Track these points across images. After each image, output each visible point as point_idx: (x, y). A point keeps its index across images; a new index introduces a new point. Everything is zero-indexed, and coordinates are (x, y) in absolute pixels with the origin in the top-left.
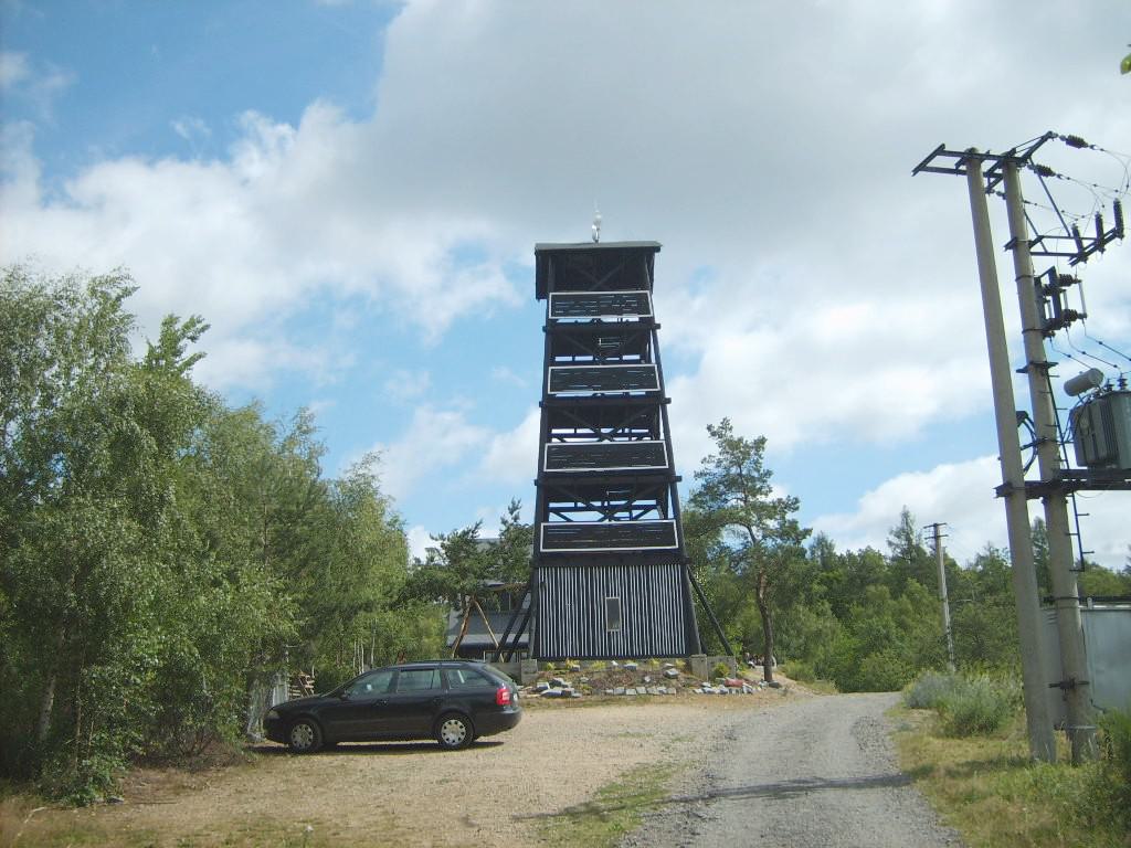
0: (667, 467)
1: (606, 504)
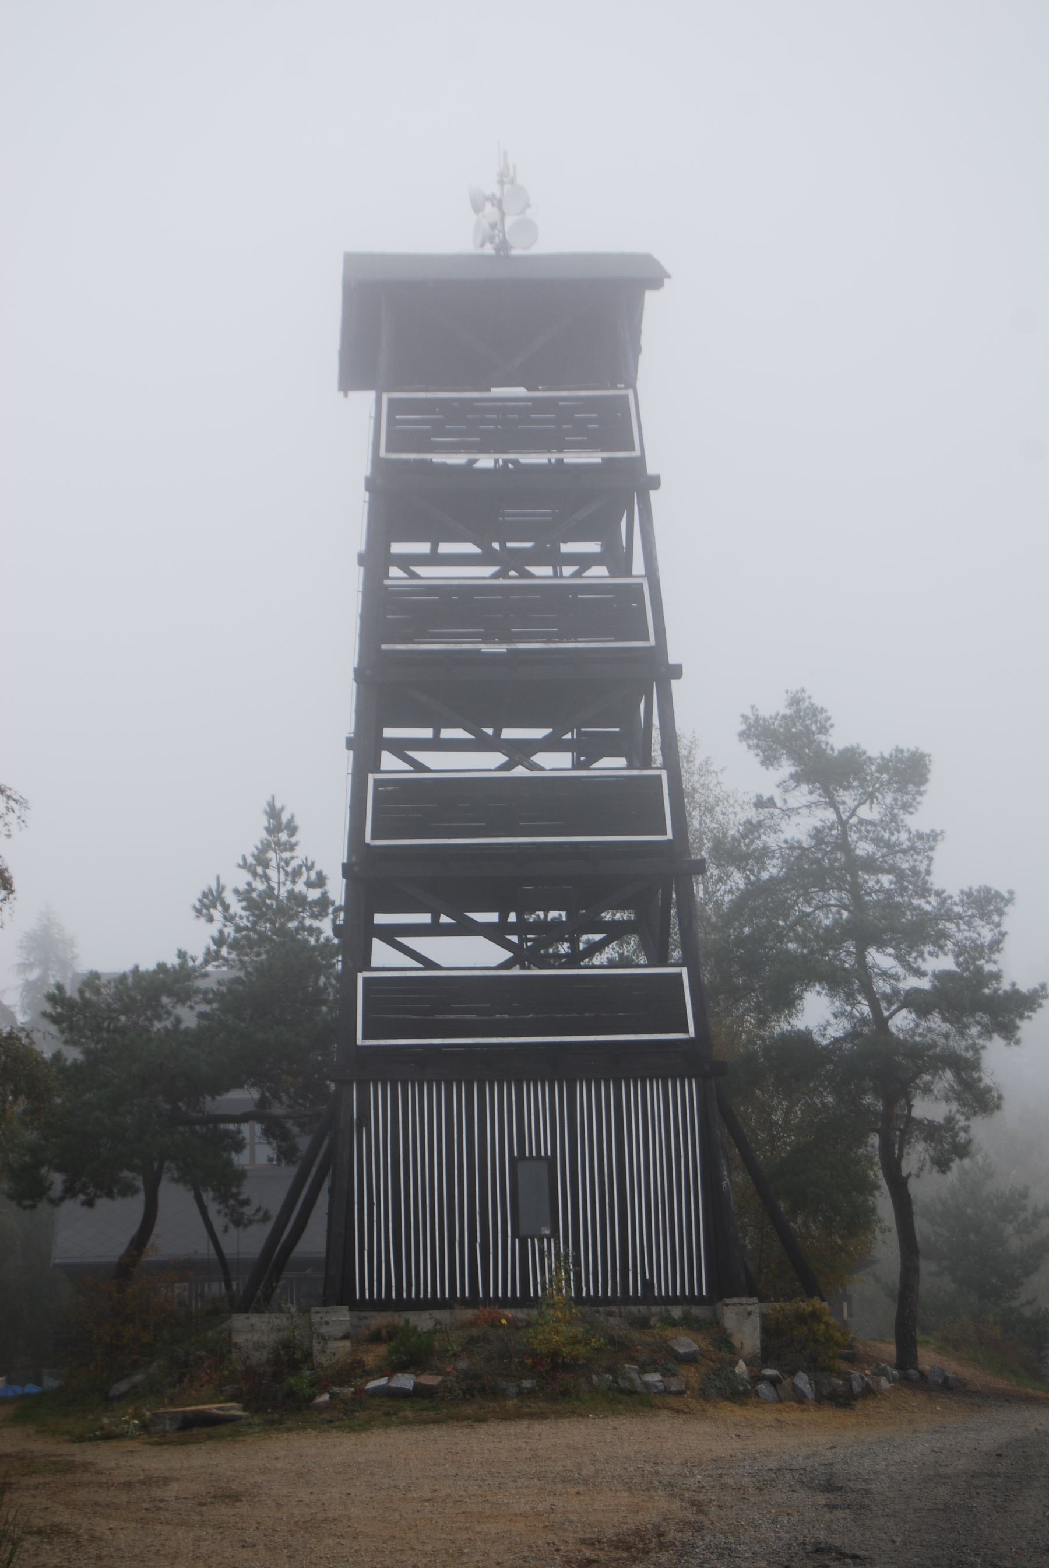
0: (652, 641)
1: (512, 917)
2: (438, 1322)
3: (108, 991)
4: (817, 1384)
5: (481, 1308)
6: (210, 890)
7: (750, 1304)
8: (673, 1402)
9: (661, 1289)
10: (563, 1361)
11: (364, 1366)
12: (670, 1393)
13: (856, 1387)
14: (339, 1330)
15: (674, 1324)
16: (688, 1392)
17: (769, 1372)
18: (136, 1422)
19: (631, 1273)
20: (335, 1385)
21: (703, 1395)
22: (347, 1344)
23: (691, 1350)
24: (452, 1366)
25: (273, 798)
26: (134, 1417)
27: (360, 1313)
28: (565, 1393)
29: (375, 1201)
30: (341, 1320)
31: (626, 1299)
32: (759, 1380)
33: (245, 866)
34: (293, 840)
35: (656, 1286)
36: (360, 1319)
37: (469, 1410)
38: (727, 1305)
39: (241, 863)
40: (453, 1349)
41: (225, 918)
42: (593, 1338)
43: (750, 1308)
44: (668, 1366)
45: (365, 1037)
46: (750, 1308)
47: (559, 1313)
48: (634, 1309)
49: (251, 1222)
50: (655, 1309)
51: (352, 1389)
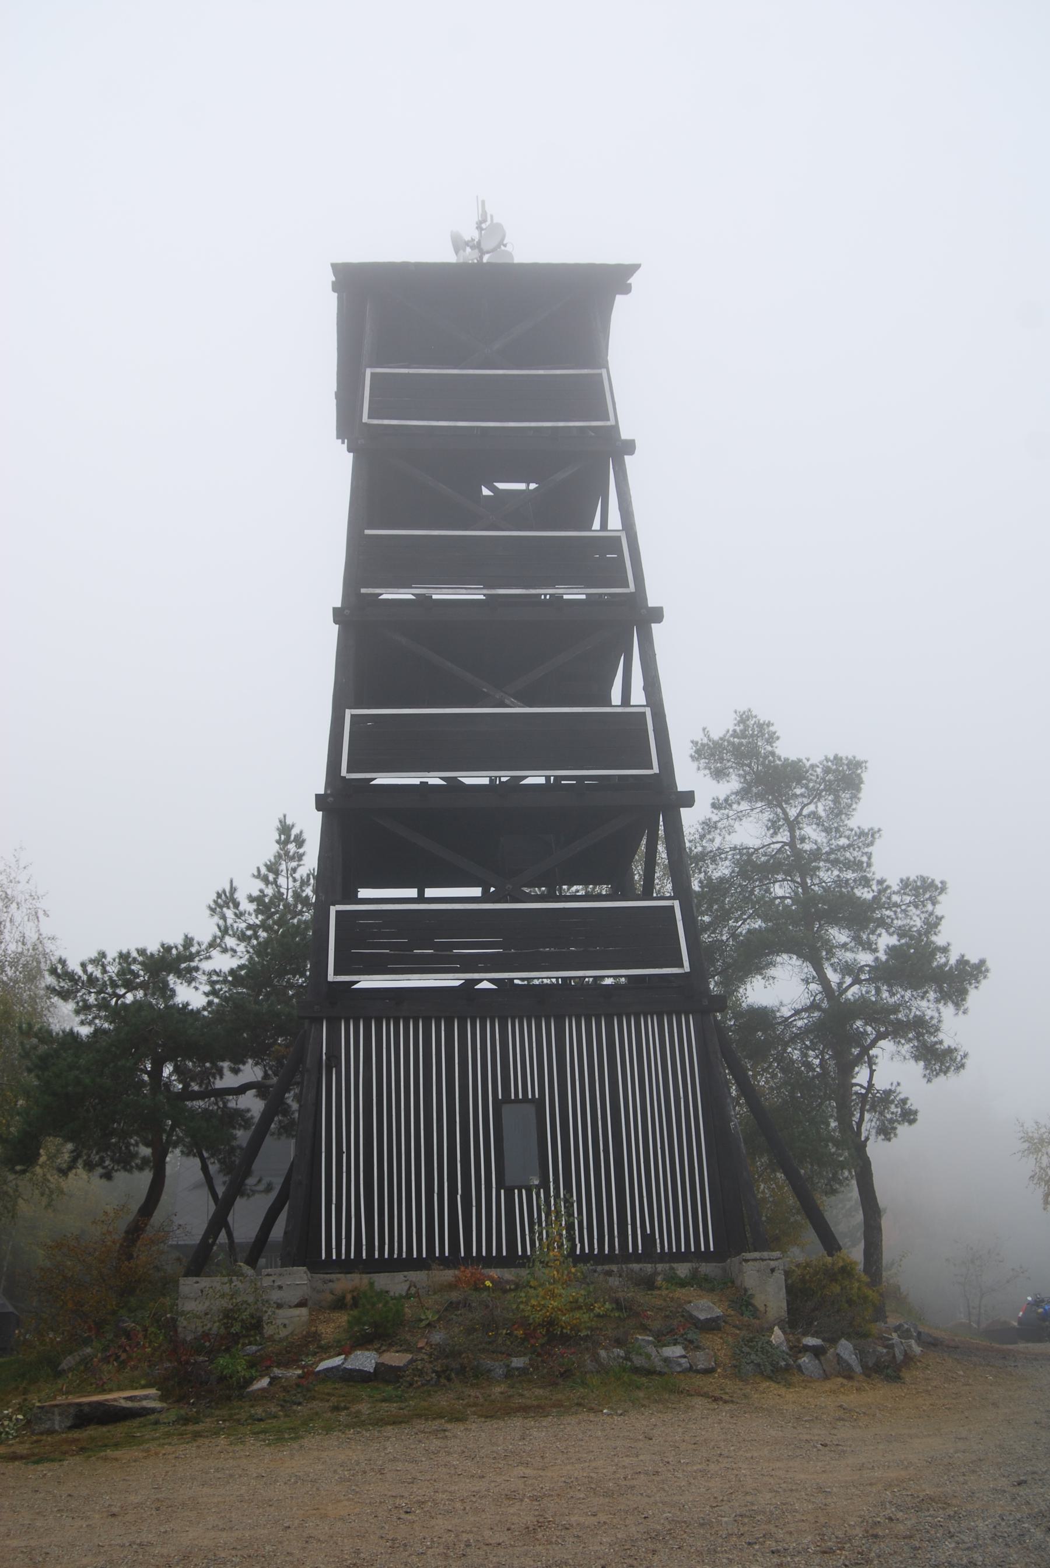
0: (632, 588)
2: (413, 1285)
3: (113, 969)
4: (861, 1353)
5: (462, 1269)
6: (224, 892)
7: (773, 1260)
8: (699, 1381)
9: (664, 1244)
10: (562, 1331)
11: (320, 1341)
12: (698, 1372)
13: (900, 1357)
14: (294, 1297)
15: (683, 1284)
16: (719, 1370)
17: (811, 1341)
18: (20, 1417)
19: (629, 1227)
20: (278, 1366)
21: (737, 1373)
22: (304, 1311)
23: (714, 1315)
24: (426, 1340)
25: (285, 816)
26: (20, 1410)
27: (325, 1276)
28: (566, 1374)
29: (344, 1149)
30: (297, 1284)
31: (626, 1257)
32: (800, 1352)
33: (258, 876)
34: (301, 851)
35: (658, 1241)
36: (325, 1282)
37: (442, 1400)
38: (747, 1261)
39: (256, 873)
40: (427, 1319)
41: (235, 914)
42: (595, 1303)
43: (773, 1264)
44: (689, 1336)
45: (336, 973)
46: (773, 1264)
47: (555, 1273)
48: (636, 1267)
49: (254, 1192)
50: (660, 1267)
51: (299, 1372)
